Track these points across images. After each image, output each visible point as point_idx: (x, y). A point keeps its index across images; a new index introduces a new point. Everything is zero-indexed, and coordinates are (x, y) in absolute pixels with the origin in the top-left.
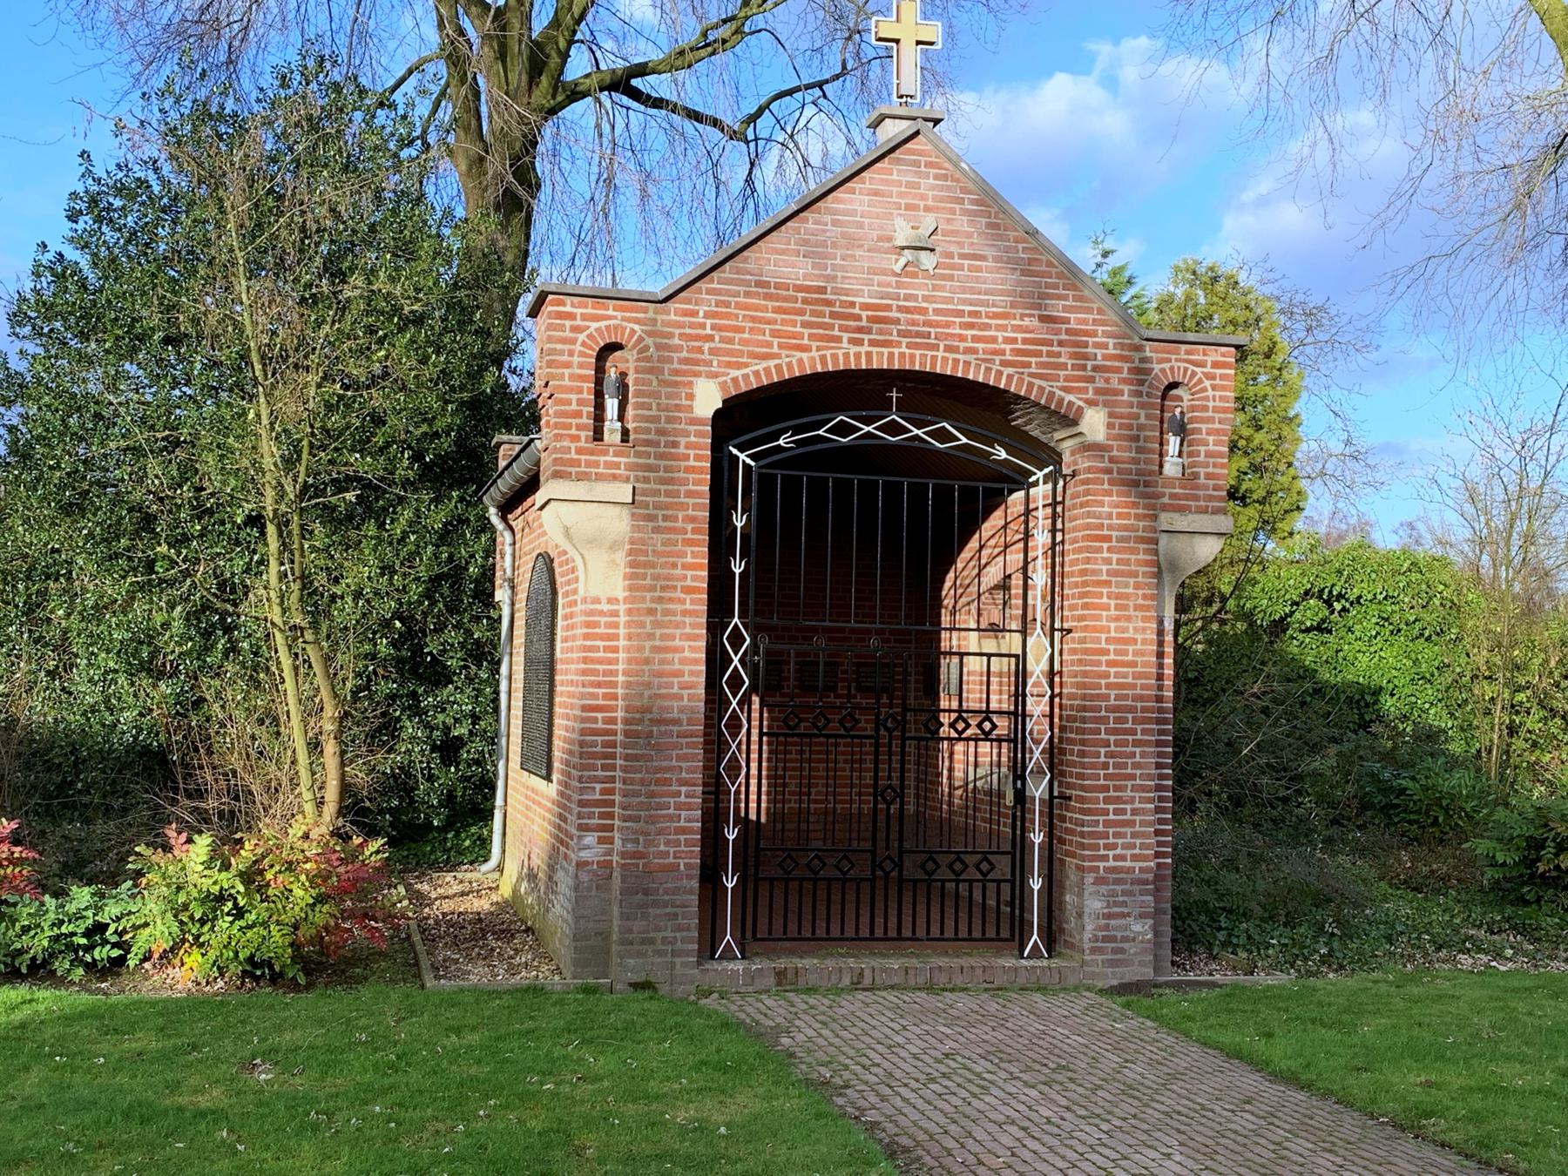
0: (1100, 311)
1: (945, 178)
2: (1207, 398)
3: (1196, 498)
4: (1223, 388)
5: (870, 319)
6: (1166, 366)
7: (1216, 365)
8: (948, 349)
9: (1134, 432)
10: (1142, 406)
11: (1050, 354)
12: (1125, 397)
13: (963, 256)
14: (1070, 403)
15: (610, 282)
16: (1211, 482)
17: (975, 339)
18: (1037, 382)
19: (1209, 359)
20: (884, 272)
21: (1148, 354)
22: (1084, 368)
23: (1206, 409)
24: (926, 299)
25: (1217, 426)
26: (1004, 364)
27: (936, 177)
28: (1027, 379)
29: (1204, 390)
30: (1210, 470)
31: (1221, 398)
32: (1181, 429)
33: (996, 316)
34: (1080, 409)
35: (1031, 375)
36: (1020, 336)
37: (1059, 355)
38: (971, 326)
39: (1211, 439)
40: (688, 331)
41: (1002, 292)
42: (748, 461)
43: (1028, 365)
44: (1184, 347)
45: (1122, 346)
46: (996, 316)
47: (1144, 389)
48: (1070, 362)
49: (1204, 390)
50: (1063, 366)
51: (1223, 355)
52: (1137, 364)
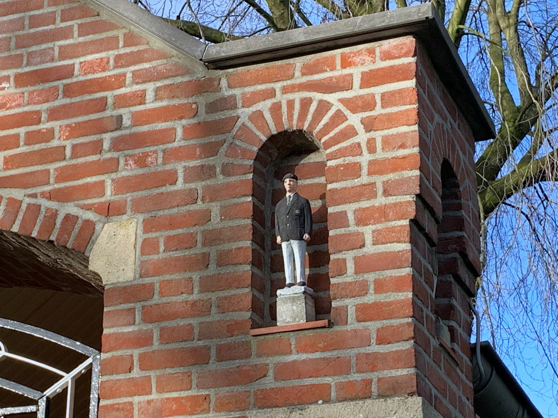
0: (130, 40)
2: (356, 149)
3: (340, 367)
4: (391, 120)
6: (264, 106)
7: (370, 79)
9: (199, 249)
10: (212, 195)
11: (31, 138)
12: (180, 185)
14: (70, 219)
15: (542, 185)
16: (373, 326)
19: (356, 72)
21: (227, 93)
22: (97, 147)
23: (354, 170)
25: (380, 200)
29: (351, 132)
30: (371, 298)
31: (387, 142)
32: (315, 229)
34: (89, 226)
37: (49, 135)
39: (368, 231)
42: (56, 388)
44: (299, 62)
45: (171, 91)
47: (218, 161)
48: (68, 144)
49: (351, 132)
50: (58, 154)
51: (387, 56)
52: (203, 116)
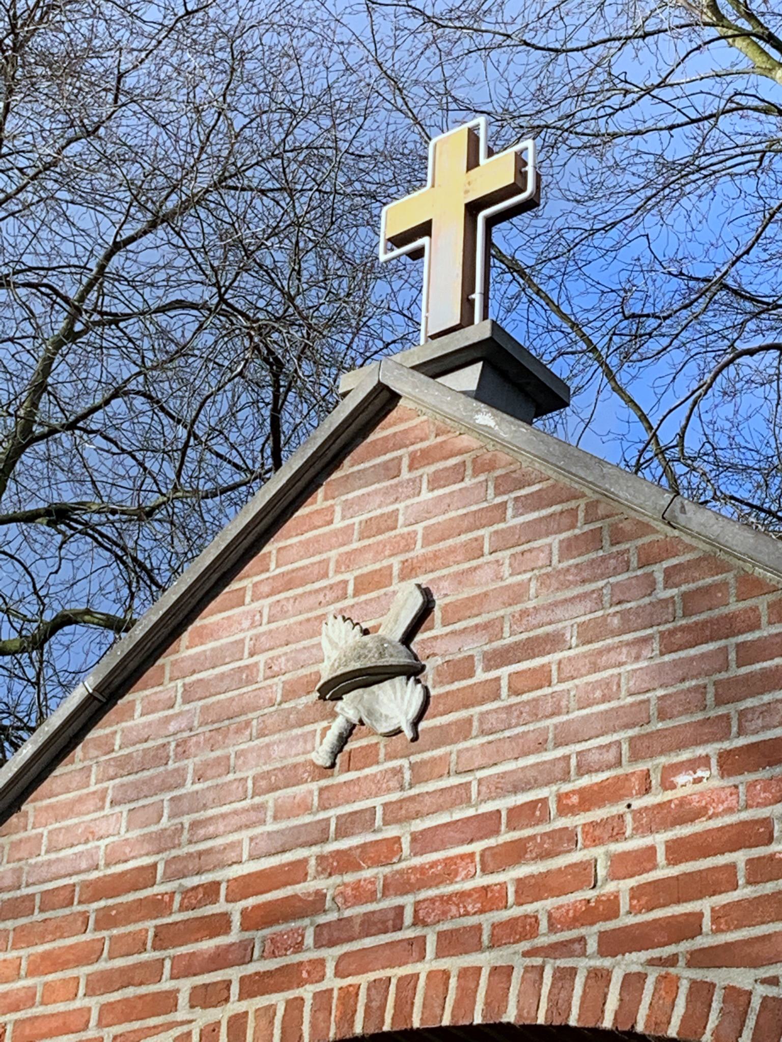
1: (458, 474)
5: (251, 920)
8: (451, 943)
13: (496, 659)
17: (530, 889)
18: (721, 977)
20: (290, 776)
24: (396, 813)
26: (613, 944)
27: (435, 482)
28: (686, 975)
33: (589, 799)
35: (698, 959)
36: (659, 839)
38: (515, 853)
40: (208, 945)
41: (610, 722)
43: (689, 927)
46: (589, 799)
